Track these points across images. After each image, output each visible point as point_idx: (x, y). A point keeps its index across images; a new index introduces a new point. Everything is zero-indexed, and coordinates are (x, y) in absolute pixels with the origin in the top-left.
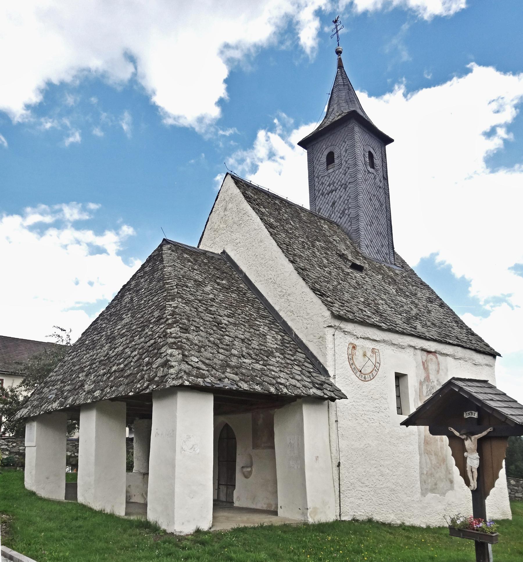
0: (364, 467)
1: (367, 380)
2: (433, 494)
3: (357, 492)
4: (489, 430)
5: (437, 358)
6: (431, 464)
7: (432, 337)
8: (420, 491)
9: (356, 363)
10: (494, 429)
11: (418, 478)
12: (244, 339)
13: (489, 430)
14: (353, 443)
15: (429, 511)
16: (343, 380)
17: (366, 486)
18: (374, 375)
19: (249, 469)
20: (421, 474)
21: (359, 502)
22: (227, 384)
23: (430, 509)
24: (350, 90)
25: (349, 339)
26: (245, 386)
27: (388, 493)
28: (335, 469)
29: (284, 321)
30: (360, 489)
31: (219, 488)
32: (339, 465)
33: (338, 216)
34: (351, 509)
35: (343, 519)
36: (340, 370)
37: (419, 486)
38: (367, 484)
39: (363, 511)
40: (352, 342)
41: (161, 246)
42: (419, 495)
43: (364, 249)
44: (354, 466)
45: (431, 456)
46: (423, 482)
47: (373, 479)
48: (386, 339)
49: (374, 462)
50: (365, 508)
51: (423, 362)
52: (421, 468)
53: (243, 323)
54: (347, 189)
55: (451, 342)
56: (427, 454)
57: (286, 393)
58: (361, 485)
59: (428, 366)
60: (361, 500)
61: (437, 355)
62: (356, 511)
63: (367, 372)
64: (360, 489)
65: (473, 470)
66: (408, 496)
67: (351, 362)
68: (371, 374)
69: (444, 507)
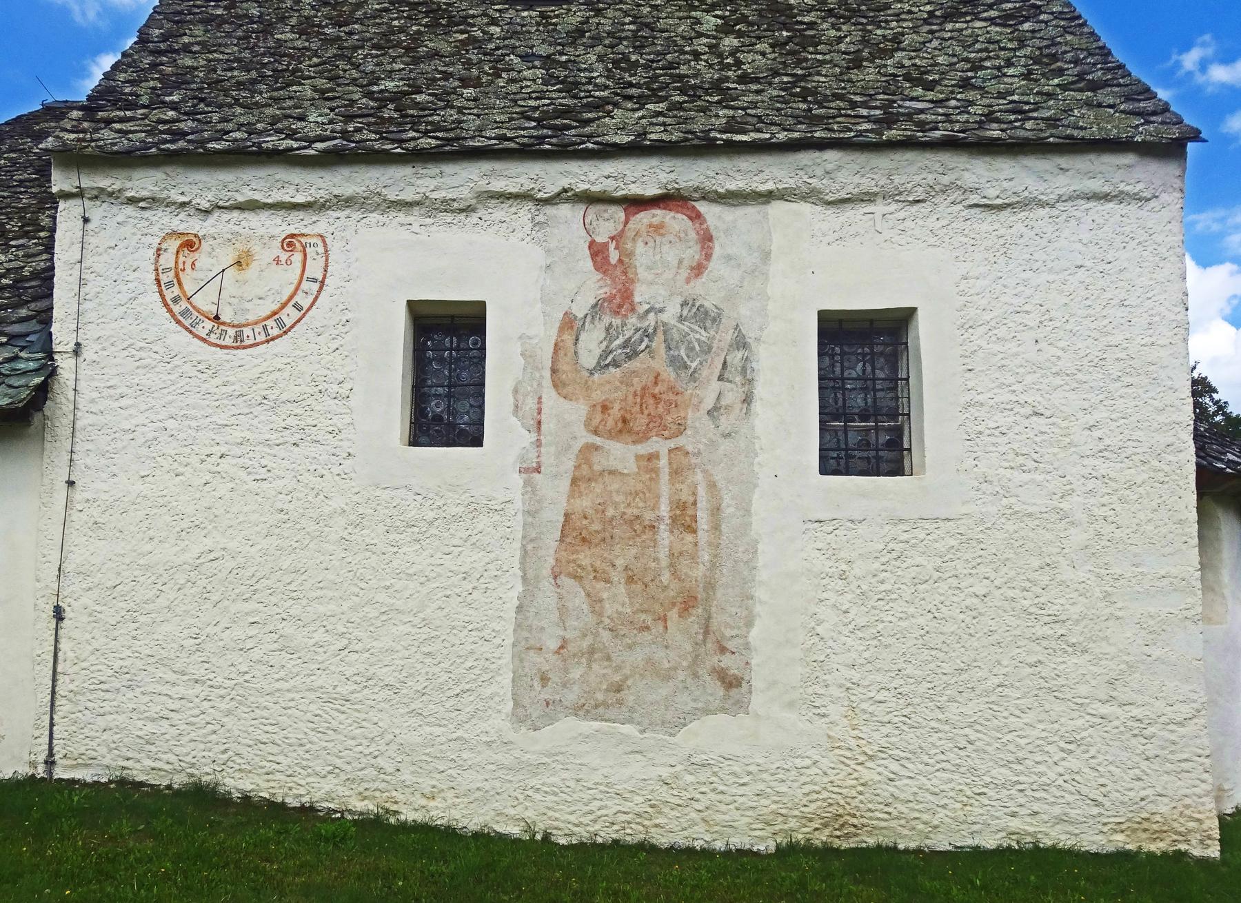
1: (247, 342)
5: (697, 217)
12: (155, 128)
18: (289, 322)
20: (526, 646)
25: (166, 220)
35: (60, 773)
40: (181, 228)
41: (1196, 405)
42: (498, 722)
48: (348, 190)
51: (592, 244)
61: (702, 207)
63: (251, 317)
68: (270, 323)
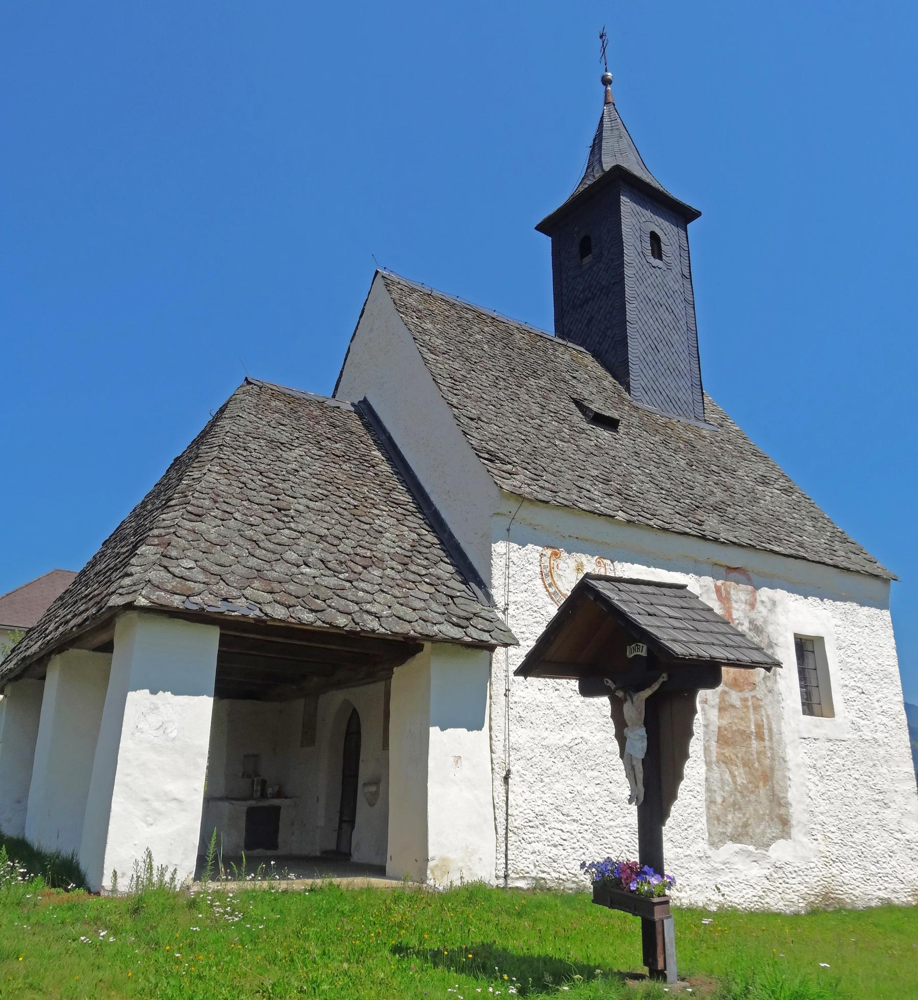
0: (569, 782)
2: (739, 845)
3: (550, 832)
4: (661, 680)
6: (735, 783)
7: (750, 542)
8: (706, 836)
9: (559, 583)
10: (669, 676)
11: (703, 810)
13: (661, 680)
14: (545, 734)
15: (727, 878)
16: (528, 613)
17: (574, 820)
19: (373, 789)
20: (711, 802)
21: (554, 851)
22: (240, 608)
23: (731, 875)
24: (621, 137)
26: (279, 613)
27: (627, 837)
28: (499, 782)
29: (436, 509)
30: (558, 826)
31: (340, 828)
32: (506, 779)
33: (597, 340)
34: (535, 866)
35: (512, 884)
36: (522, 595)
37: (705, 827)
38: (576, 815)
39: (564, 870)
43: (639, 394)
44: (546, 780)
45: (734, 768)
46: (715, 819)
47: (592, 807)
49: (595, 773)
50: (568, 866)
52: (708, 790)
53: (341, 511)
54: (610, 295)
55: (776, 549)
56: (725, 763)
57: (373, 631)
58: (562, 818)
59: (728, 593)
60: (560, 848)
62: (546, 869)
64: (558, 826)
65: (634, 763)
66: (676, 847)
67: (548, 581)
69: (767, 872)
